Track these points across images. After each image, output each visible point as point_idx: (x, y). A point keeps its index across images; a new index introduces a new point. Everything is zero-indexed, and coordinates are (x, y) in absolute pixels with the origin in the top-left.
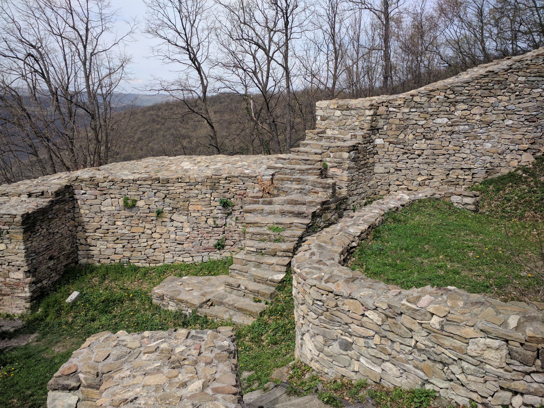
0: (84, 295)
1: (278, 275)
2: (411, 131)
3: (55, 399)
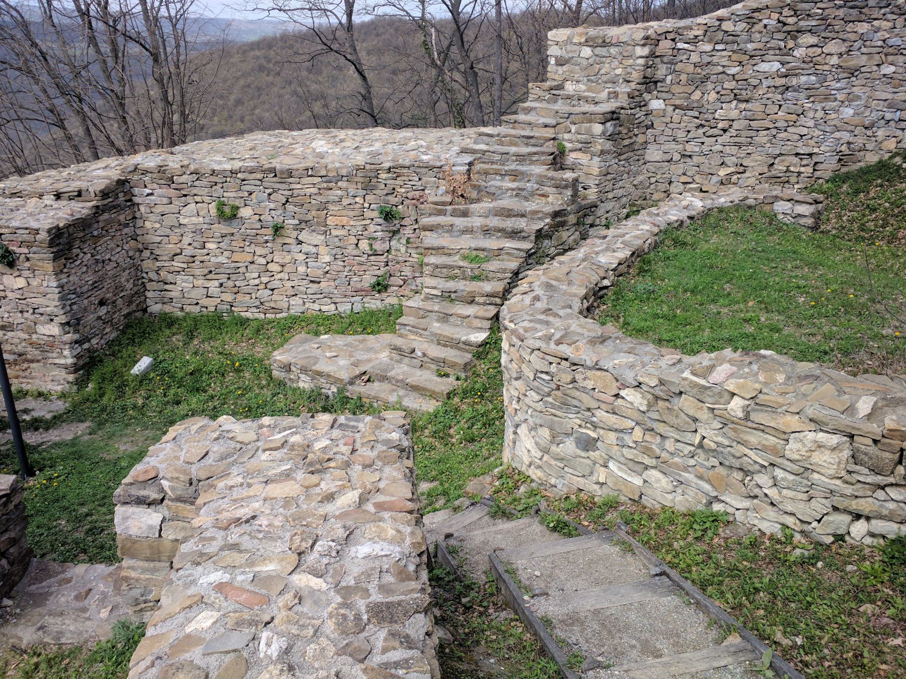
0: (160, 362)
1: (477, 335)
2: (713, 86)
3: (127, 518)
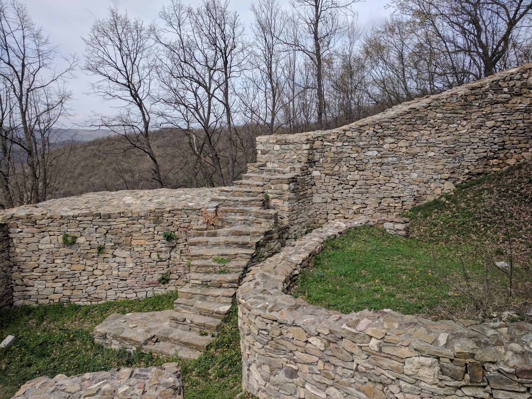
0: (20, 339)
2: (345, 163)
